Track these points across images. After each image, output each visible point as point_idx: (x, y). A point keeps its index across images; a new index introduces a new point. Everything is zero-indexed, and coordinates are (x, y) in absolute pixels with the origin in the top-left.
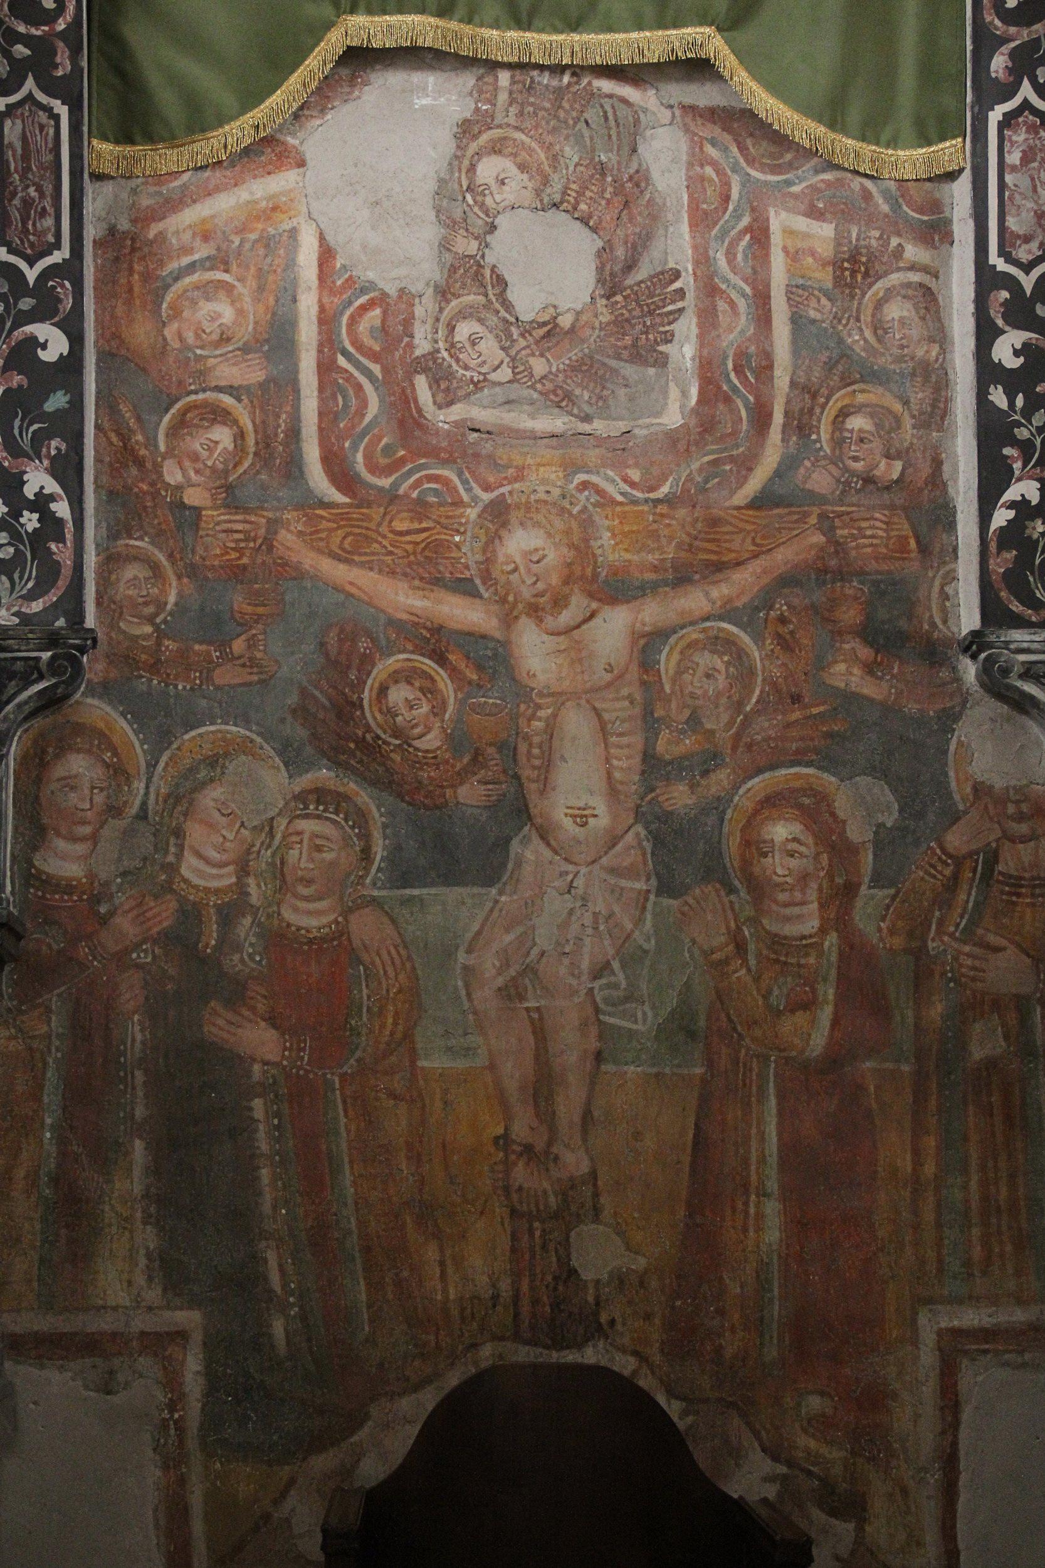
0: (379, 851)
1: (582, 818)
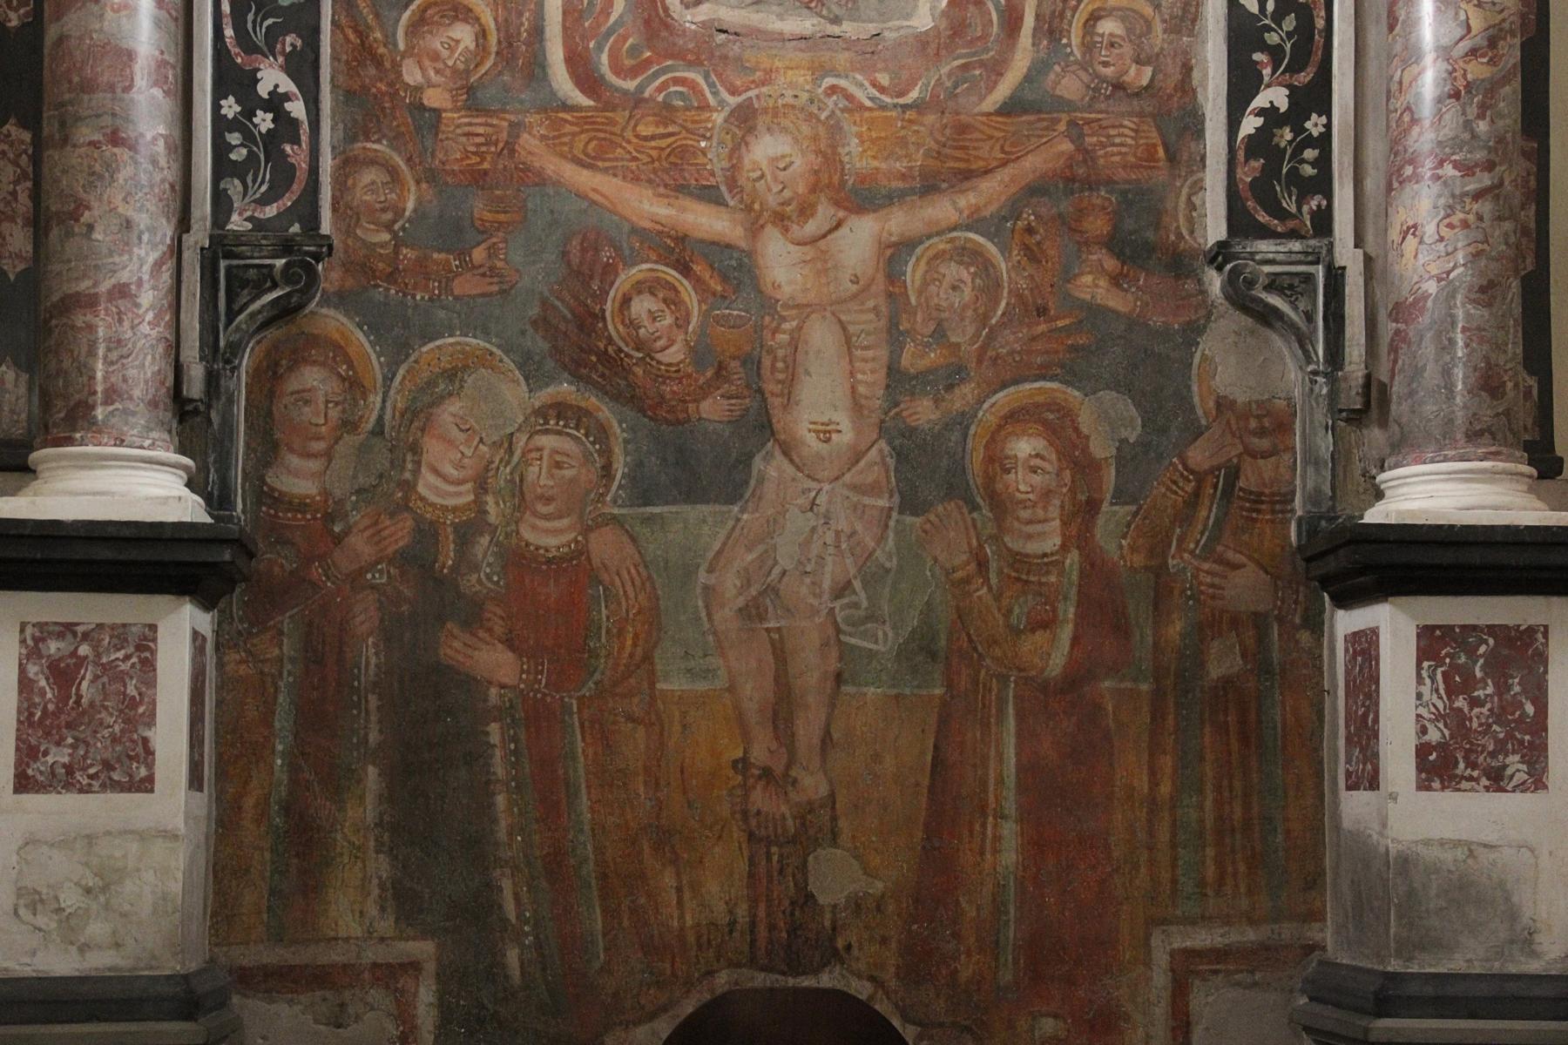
0: (620, 469)
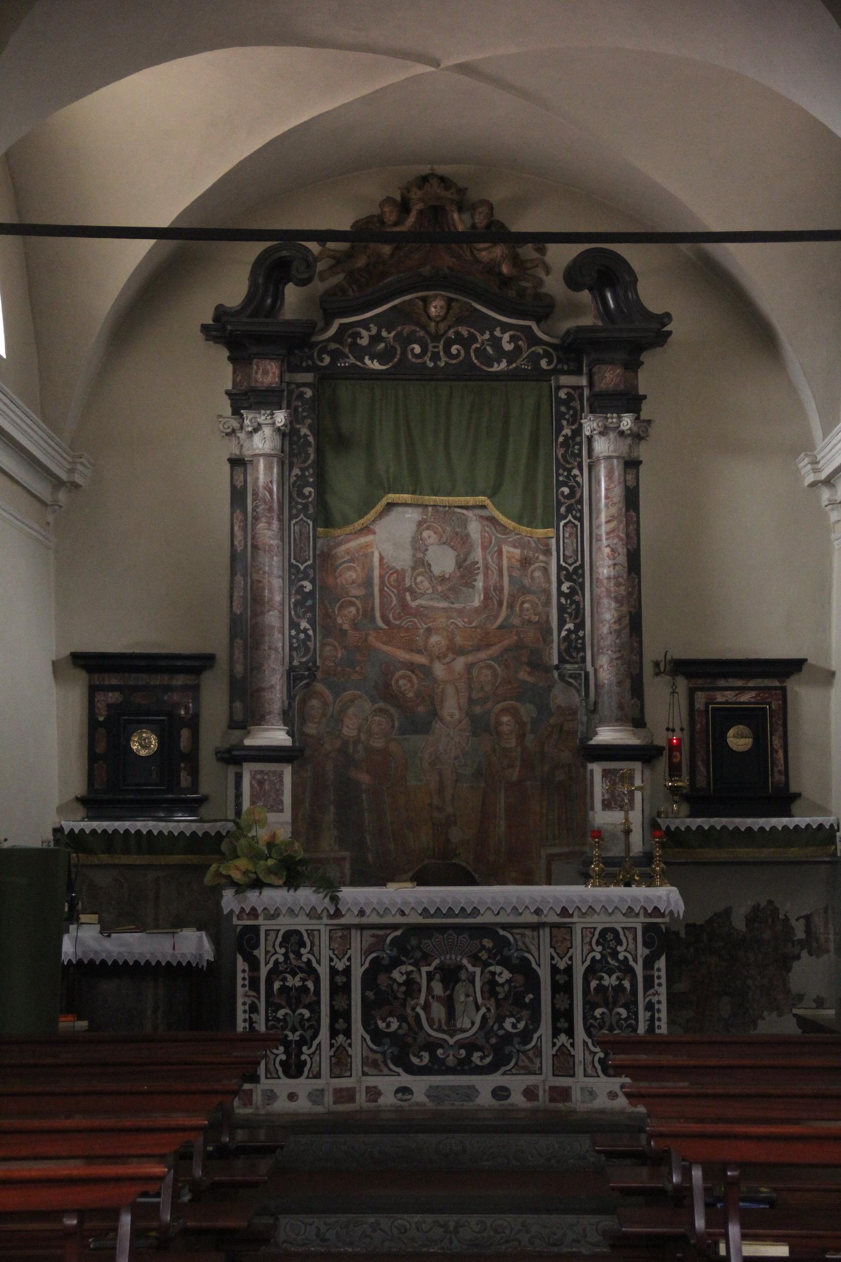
0: (396, 724)
1: (452, 716)
